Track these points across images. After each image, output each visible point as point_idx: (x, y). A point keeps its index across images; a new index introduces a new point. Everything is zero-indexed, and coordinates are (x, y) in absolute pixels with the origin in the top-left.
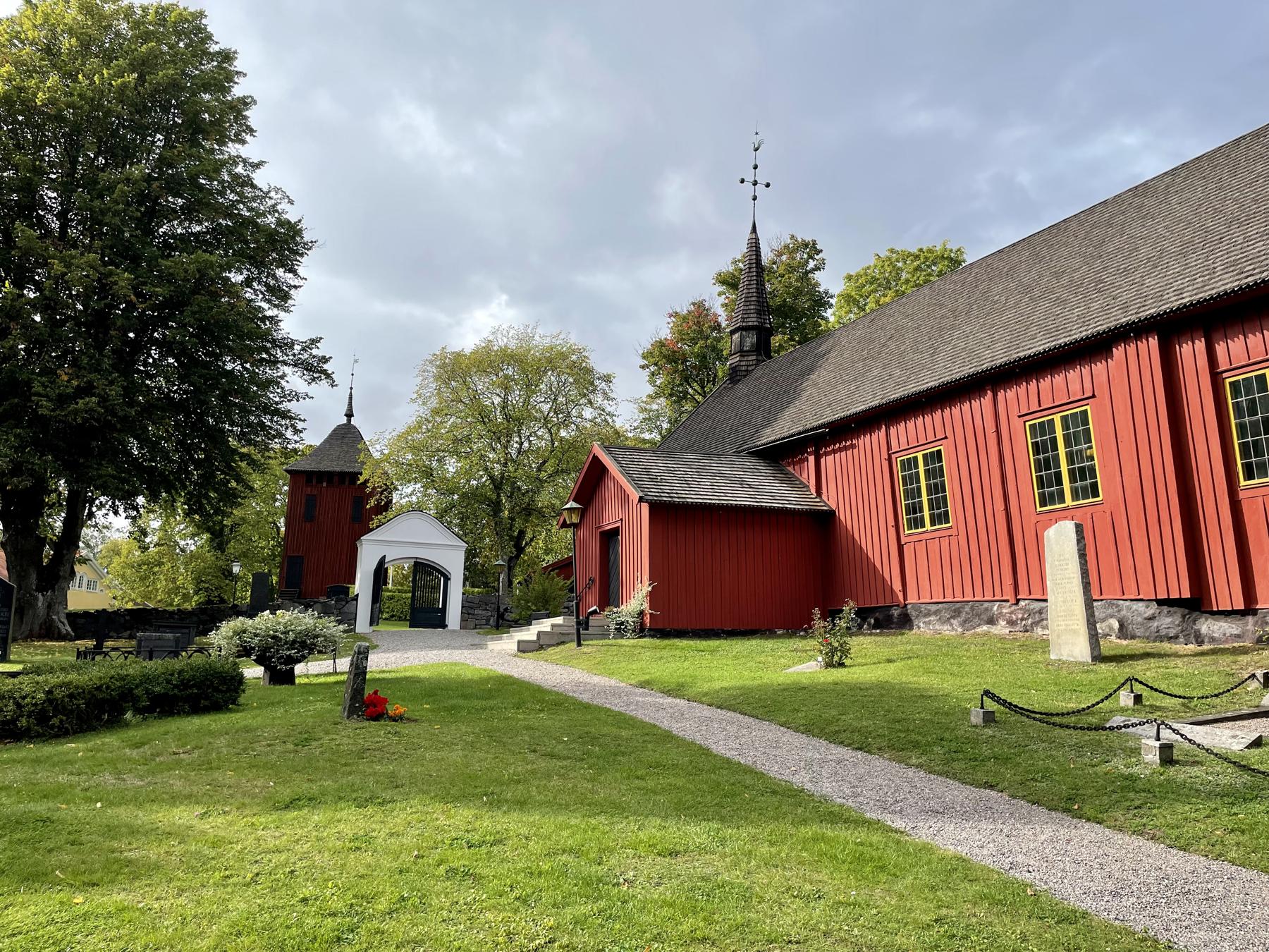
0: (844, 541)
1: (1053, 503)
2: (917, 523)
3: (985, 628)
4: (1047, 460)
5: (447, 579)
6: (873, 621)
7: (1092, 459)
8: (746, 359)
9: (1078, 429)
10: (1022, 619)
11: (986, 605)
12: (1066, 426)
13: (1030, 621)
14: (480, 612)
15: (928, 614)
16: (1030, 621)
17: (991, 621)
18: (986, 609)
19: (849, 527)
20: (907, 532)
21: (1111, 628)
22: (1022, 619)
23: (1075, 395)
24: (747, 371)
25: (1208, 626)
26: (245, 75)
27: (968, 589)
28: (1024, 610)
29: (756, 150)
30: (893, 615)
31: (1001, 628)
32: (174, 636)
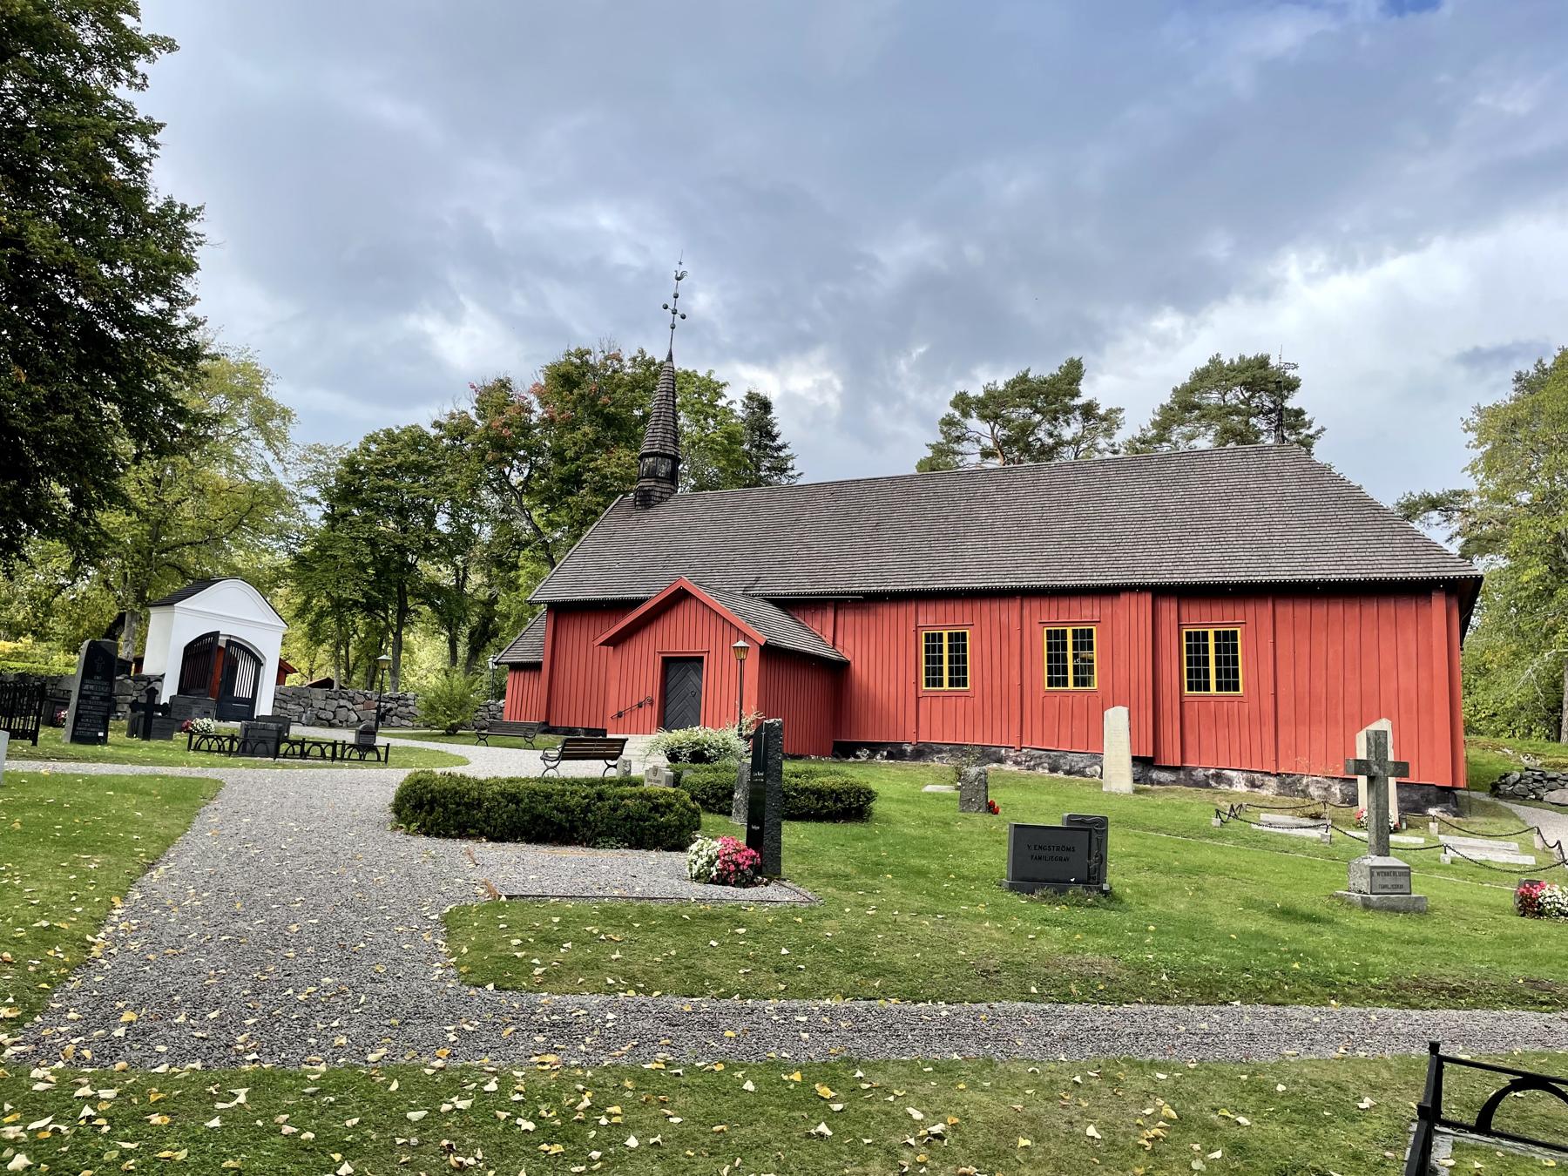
0: (856, 689)
1: (1058, 685)
2: (935, 681)
3: (995, 765)
4: (1057, 656)
5: (258, 663)
6: (885, 753)
7: (1092, 661)
8: (660, 485)
9: (1084, 640)
10: (1026, 761)
11: (994, 749)
12: (1075, 636)
13: (1032, 763)
14: (293, 707)
15: (940, 751)
16: (1032, 763)
17: (1000, 761)
18: (995, 752)
19: (865, 678)
20: (924, 688)
21: (1096, 772)
22: (1026, 761)
23: (1086, 617)
24: (661, 497)
25: (1155, 775)
26: (170, 45)
27: (1246, 755)
28: (1027, 755)
29: (678, 279)
30: (906, 750)
31: (1009, 767)
32: (277, 727)
